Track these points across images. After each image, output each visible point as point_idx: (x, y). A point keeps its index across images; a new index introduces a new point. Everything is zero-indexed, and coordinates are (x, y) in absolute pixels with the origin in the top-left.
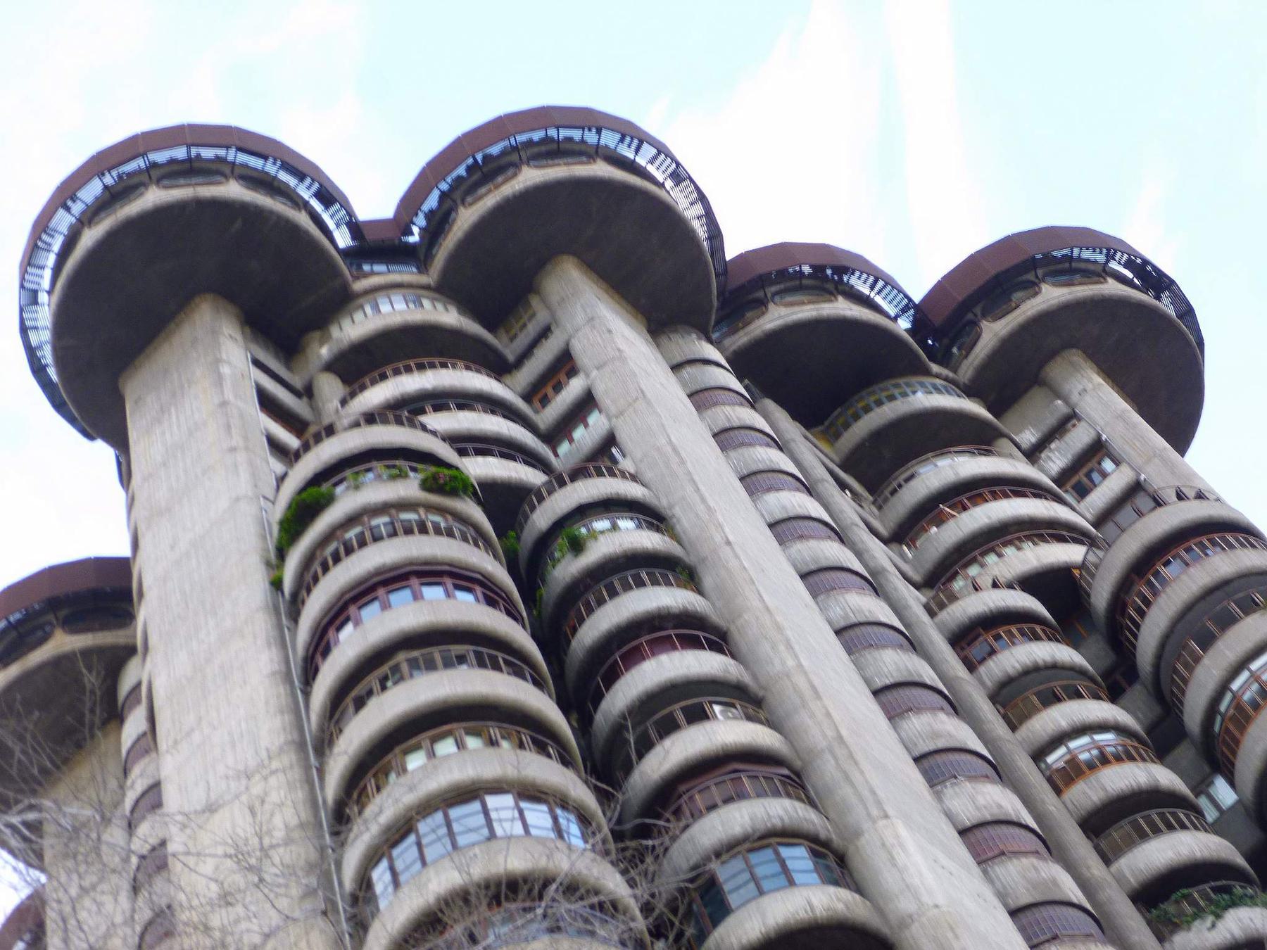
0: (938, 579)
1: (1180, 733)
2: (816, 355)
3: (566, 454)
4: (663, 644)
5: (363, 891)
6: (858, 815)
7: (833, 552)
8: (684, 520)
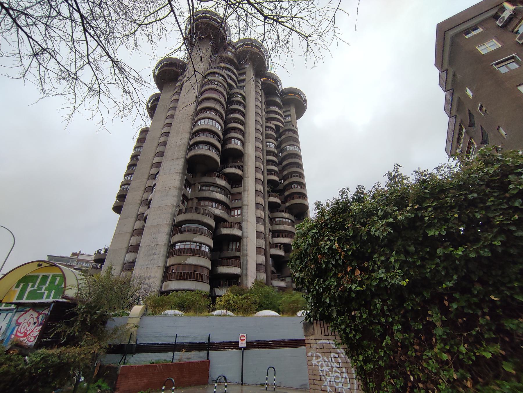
0: (269, 120)
1: (280, 147)
2: (270, 88)
3: (239, 85)
4: (239, 113)
5: (197, 122)
6: (247, 141)
7: (260, 112)
8: (247, 100)
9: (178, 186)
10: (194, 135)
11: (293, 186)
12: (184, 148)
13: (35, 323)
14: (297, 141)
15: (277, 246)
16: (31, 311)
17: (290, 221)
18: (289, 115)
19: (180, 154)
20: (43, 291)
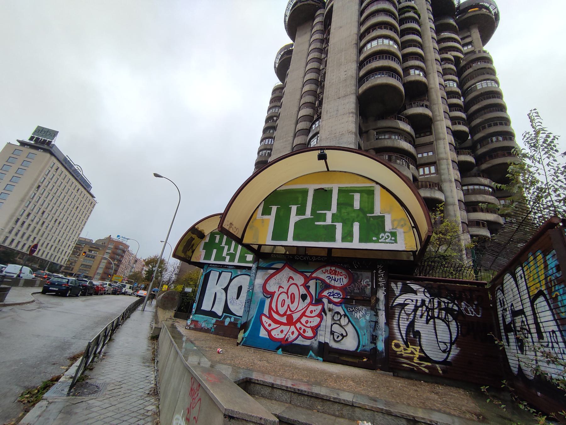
9: (354, 130)
10: (361, 65)
11: (494, 139)
12: (353, 82)
13: (304, 297)
14: (492, 72)
15: (478, 223)
16: (287, 269)
17: (490, 190)
18: (470, 43)
19: (348, 90)
20: (329, 221)
